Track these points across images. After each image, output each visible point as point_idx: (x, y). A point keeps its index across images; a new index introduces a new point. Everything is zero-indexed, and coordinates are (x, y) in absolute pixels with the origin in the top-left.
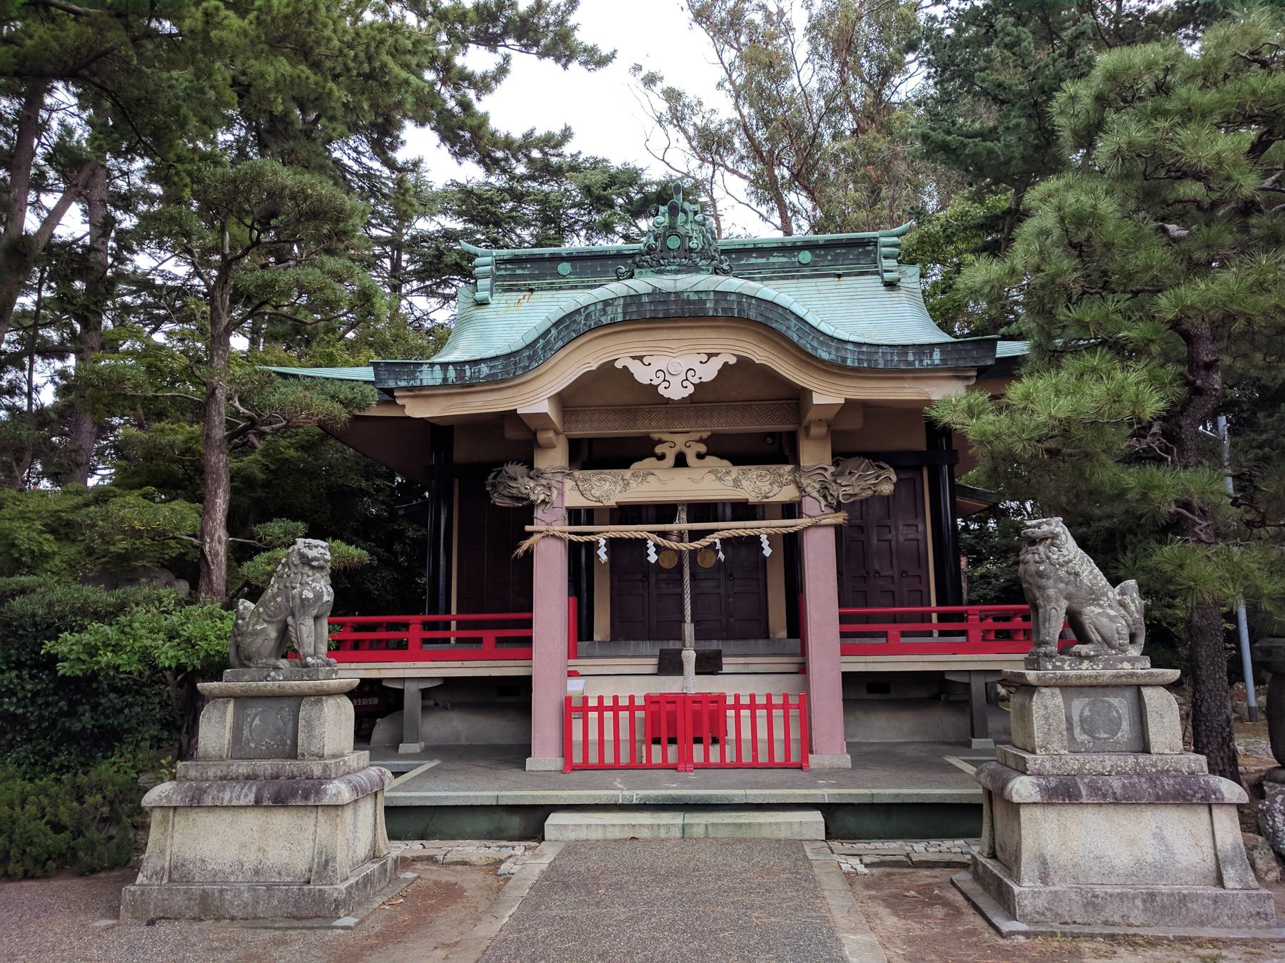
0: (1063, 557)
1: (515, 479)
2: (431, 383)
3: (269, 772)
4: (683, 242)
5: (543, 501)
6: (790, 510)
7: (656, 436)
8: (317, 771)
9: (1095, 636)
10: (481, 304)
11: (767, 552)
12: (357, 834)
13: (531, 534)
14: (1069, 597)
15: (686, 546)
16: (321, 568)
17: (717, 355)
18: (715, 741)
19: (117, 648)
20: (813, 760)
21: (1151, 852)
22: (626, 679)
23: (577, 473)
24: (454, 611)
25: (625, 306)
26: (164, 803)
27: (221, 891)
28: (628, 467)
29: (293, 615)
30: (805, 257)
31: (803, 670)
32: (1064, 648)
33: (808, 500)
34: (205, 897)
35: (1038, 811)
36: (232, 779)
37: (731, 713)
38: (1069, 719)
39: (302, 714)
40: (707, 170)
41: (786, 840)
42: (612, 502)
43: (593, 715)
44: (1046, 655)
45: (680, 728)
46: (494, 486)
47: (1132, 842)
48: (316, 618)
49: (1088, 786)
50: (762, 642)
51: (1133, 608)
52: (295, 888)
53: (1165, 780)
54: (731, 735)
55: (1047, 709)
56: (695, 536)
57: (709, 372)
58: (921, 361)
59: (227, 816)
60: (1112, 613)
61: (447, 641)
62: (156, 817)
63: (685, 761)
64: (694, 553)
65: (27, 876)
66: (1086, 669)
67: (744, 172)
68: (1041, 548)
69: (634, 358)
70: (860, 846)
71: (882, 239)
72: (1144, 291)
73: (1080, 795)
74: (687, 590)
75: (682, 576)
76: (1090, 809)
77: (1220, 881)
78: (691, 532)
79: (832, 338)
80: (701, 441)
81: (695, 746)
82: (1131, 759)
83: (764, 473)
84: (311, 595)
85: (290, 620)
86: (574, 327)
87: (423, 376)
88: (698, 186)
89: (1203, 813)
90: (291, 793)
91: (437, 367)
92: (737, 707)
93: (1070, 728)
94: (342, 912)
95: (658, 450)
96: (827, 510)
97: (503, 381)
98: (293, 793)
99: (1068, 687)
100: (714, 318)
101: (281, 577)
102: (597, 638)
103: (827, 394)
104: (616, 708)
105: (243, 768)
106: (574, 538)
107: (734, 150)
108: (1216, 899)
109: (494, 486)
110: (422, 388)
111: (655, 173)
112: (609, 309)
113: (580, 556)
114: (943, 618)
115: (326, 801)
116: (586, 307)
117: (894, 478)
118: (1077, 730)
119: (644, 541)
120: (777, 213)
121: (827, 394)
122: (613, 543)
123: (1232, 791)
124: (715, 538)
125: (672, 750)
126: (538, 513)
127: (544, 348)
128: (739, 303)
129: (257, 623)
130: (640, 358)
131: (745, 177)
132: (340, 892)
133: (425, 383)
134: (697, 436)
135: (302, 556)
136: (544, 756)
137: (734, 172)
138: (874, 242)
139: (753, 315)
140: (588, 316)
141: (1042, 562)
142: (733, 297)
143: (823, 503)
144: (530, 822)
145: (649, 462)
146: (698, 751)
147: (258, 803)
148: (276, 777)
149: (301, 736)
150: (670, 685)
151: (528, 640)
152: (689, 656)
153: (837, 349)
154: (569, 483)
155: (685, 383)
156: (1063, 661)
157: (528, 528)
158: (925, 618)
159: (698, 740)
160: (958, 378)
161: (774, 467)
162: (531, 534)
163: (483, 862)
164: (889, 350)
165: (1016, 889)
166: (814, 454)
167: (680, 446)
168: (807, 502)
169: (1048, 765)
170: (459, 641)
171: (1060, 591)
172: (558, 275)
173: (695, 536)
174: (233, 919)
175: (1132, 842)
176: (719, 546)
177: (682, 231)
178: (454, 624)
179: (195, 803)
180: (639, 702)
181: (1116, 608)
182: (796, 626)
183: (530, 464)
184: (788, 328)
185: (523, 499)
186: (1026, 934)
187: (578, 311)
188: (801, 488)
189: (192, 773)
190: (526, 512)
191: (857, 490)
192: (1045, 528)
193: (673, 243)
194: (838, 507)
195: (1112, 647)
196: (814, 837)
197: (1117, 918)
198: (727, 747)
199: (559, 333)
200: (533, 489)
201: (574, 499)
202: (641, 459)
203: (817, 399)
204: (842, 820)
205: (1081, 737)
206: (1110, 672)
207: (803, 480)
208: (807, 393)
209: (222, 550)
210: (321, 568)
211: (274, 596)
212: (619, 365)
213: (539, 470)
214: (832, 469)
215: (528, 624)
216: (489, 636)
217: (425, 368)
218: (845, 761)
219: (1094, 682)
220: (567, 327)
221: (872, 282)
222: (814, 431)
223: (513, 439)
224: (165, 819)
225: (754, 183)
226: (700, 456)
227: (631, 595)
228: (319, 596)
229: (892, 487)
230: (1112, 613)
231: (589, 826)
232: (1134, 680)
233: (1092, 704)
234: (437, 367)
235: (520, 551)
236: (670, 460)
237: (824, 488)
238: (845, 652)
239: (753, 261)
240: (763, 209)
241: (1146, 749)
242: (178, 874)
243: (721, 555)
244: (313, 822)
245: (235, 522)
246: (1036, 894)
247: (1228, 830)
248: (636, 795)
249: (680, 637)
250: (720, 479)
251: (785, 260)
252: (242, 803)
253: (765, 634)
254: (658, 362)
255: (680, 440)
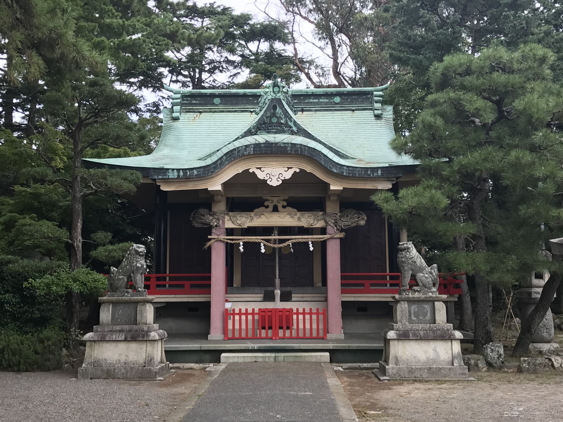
0: (413, 254)
1: (204, 216)
2: (172, 177)
3: (128, 329)
4: (278, 120)
5: (216, 225)
6: (323, 231)
7: (265, 198)
8: (146, 329)
9: (420, 284)
10: (176, 119)
11: (312, 249)
12: (157, 352)
13: (211, 239)
14: (412, 270)
15: (277, 246)
16: (142, 256)
17: (291, 168)
18: (288, 328)
19: (57, 285)
20: (329, 336)
21: (432, 355)
22: (250, 304)
23: (230, 213)
24: (168, 272)
25: (254, 148)
26: (91, 339)
27: (114, 369)
28: (252, 211)
29: (133, 273)
30: (337, 99)
31: (326, 300)
32: (411, 286)
33: (327, 231)
34: (108, 371)
35: (396, 342)
36: (114, 331)
37: (295, 317)
38: (410, 312)
39: (138, 309)
40: (290, 17)
41: (315, 362)
42: (246, 226)
43: (237, 317)
44: (403, 290)
45: (272, 322)
46: (194, 218)
47: (426, 352)
48: (141, 274)
49: (413, 333)
50: (310, 288)
51: (434, 274)
52: (141, 368)
53: (438, 332)
54: (295, 327)
55: (402, 309)
56: (281, 241)
57: (288, 175)
58: (373, 174)
59: (114, 344)
60: (427, 276)
61: (165, 286)
62: (88, 344)
63: (275, 337)
64: (280, 249)
65: (27, 371)
66: (416, 295)
67: (312, 19)
68: (404, 253)
69: (257, 168)
70: (341, 365)
71: (375, 93)
72: (450, 153)
73: (409, 336)
74: (277, 265)
75: (275, 258)
76: (413, 341)
77: (453, 365)
78: (279, 240)
79: (338, 164)
80: (284, 200)
81: (280, 330)
82: (428, 325)
83: (311, 215)
84: (140, 266)
85: (132, 275)
86: (233, 156)
87: (170, 174)
88: (283, 25)
89: (450, 343)
90: (138, 336)
91: (175, 171)
92: (298, 313)
93: (410, 315)
94: (157, 376)
95: (266, 204)
96: (337, 232)
97: (203, 177)
98: (139, 336)
99: (410, 301)
100: (290, 154)
101: (128, 258)
102: (235, 285)
103: (335, 187)
104: (246, 314)
105: (118, 328)
106: (229, 241)
107: (306, 6)
108: (450, 369)
109: (194, 218)
110: (168, 179)
111: (259, 18)
112: (248, 149)
113: (230, 249)
114: (392, 278)
115: (150, 339)
116: (238, 148)
117: (366, 218)
118: (412, 316)
119: (259, 243)
120: (330, 46)
121: (335, 187)
122: (244, 243)
123: (458, 334)
124: (290, 243)
125: (270, 332)
126: (214, 231)
127: (220, 164)
128: (301, 148)
129: (119, 275)
130: (260, 168)
131: (312, 22)
132: (157, 369)
133: (170, 177)
134: (283, 198)
135: (136, 251)
136: (216, 333)
137: (305, 18)
138: (371, 93)
139: (306, 153)
140: (239, 152)
141: (403, 257)
142: (298, 146)
143: (335, 228)
144: (214, 356)
145: (262, 209)
146: (281, 333)
147: (125, 340)
148: (130, 331)
149: (138, 316)
150: (269, 305)
151: (210, 286)
152: (278, 292)
153: (340, 168)
154: (227, 218)
155: (278, 179)
156: (409, 292)
157: (209, 237)
158: (384, 278)
159: (281, 328)
160: (389, 181)
161: (315, 212)
162: (211, 239)
163: (199, 368)
164: (360, 169)
165: (387, 367)
166: (332, 207)
167: (275, 202)
168: (329, 227)
169: (401, 327)
170: (170, 286)
171: (409, 268)
172: (213, 104)
173: (281, 241)
174: (119, 378)
175: (426, 352)
176: (291, 246)
177: (278, 115)
178: (168, 278)
179: (103, 340)
180: (256, 311)
181: (429, 274)
182: (324, 282)
183: (210, 210)
184: (321, 159)
185: (207, 224)
186: (388, 380)
187: (234, 149)
188: (326, 222)
189: (99, 329)
190: (209, 230)
191: (350, 223)
192: (405, 245)
193: (274, 120)
194: (342, 231)
195: (426, 288)
196: (325, 361)
197: (419, 376)
198: (293, 331)
199: (227, 158)
200: (212, 220)
201: (229, 225)
202: (258, 208)
203: (332, 188)
204: (336, 355)
205: (414, 318)
206: (423, 296)
207: (327, 219)
208: (327, 185)
209: (80, 245)
210: (142, 256)
211: (126, 266)
212: (251, 171)
213: (214, 212)
214: (340, 214)
215: (209, 278)
216: (187, 283)
217: (170, 171)
218: (342, 336)
219: (419, 299)
220: (230, 156)
221: (369, 114)
222: (332, 198)
223: (206, 200)
224: (91, 346)
225: (318, 25)
226: (284, 207)
227: (251, 269)
228: (142, 266)
229: (365, 222)
230: (427, 276)
231: (238, 357)
232: (431, 299)
233: (418, 307)
234: (175, 171)
235: (206, 247)
236: (271, 208)
237: (336, 224)
238: (343, 292)
239: (311, 100)
240: (322, 43)
241: (435, 323)
242: (96, 364)
243: (292, 250)
244: (145, 346)
245: (85, 233)
246: (393, 368)
247: (457, 347)
248: (256, 346)
249: (274, 285)
250: (292, 217)
251: (327, 100)
252: (120, 339)
253: (312, 284)
254: (267, 170)
255: (275, 200)
